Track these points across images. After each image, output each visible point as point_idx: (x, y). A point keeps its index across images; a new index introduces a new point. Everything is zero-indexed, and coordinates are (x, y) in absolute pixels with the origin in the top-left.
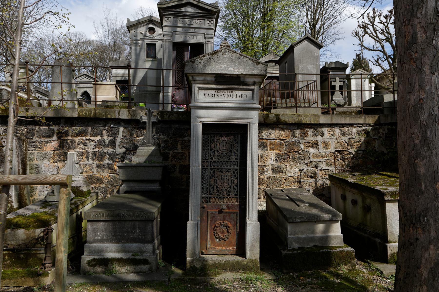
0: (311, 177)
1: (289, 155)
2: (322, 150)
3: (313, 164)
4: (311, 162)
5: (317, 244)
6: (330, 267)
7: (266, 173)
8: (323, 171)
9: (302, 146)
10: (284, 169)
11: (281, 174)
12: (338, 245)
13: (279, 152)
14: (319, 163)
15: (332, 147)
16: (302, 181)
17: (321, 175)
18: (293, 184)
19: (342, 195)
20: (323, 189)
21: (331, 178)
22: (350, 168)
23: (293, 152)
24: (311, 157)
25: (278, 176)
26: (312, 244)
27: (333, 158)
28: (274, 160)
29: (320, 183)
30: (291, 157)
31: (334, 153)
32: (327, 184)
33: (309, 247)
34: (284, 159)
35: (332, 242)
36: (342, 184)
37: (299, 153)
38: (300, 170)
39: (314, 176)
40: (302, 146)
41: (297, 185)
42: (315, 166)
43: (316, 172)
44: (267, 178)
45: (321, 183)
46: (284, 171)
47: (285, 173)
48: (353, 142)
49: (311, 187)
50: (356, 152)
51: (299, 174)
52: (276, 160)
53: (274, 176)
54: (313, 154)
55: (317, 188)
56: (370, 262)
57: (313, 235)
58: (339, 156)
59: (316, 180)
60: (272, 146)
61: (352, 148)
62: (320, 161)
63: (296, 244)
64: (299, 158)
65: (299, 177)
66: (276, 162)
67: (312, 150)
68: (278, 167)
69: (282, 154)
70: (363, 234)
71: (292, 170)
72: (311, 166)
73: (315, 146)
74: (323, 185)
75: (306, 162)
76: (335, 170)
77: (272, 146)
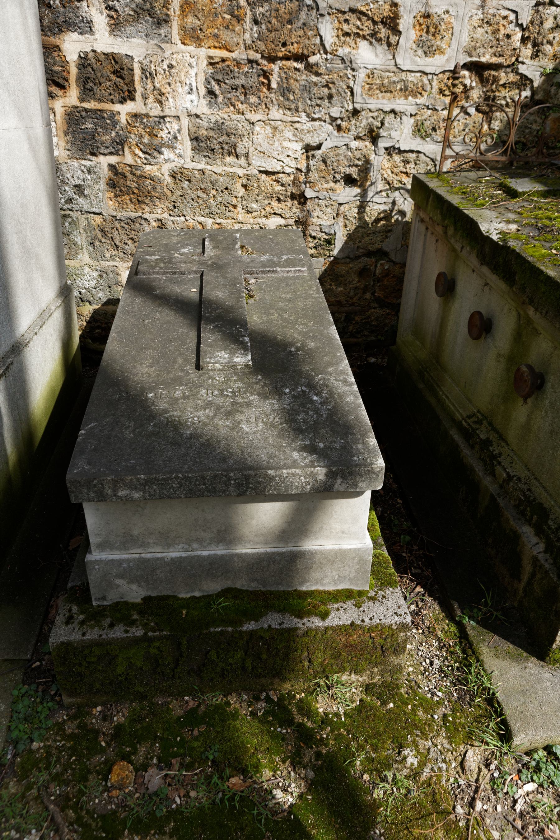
0: (349, 181)
1: (266, 74)
2: (409, 57)
3: (364, 121)
4: (356, 113)
5: (241, 584)
6: (284, 680)
7: (167, 153)
8: (397, 158)
9: (328, 30)
10: (241, 136)
11: (229, 159)
12: (341, 586)
13: (224, 54)
14: (389, 119)
15: (454, 45)
16: (309, 193)
17: (388, 174)
18: (275, 204)
19: (441, 275)
20: (387, 231)
21: (419, 189)
22: (505, 153)
23: (287, 58)
24: (357, 90)
25: (218, 170)
26: (213, 586)
27: (447, 100)
28: (203, 91)
29: (377, 206)
30: (274, 85)
31: (454, 74)
32: (402, 213)
33: (197, 594)
34: (246, 90)
35: (315, 575)
36: (451, 231)
37: (309, 67)
38: (308, 148)
39: (358, 178)
40: (328, 30)
41: (292, 210)
42: (371, 131)
43: (367, 161)
44: (173, 176)
45: (382, 207)
46: (241, 150)
47: (247, 156)
48: (549, 24)
49: (341, 220)
50: (548, 77)
51: (303, 166)
52: (211, 93)
53: (201, 166)
54: (371, 75)
55: (362, 225)
56: (470, 624)
57: (220, 551)
58: (476, 94)
59: (364, 194)
60: (191, 21)
61: (535, 56)
62: (393, 111)
63: (134, 587)
64: (307, 89)
65: (302, 178)
66: (210, 104)
67: (367, 55)
68: (219, 127)
69: (238, 64)
70: (478, 467)
71: (276, 141)
72: (353, 133)
73: (383, 32)
74: (387, 216)
75: (335, 112)
76: (444, 158)
77: (191, 21)
